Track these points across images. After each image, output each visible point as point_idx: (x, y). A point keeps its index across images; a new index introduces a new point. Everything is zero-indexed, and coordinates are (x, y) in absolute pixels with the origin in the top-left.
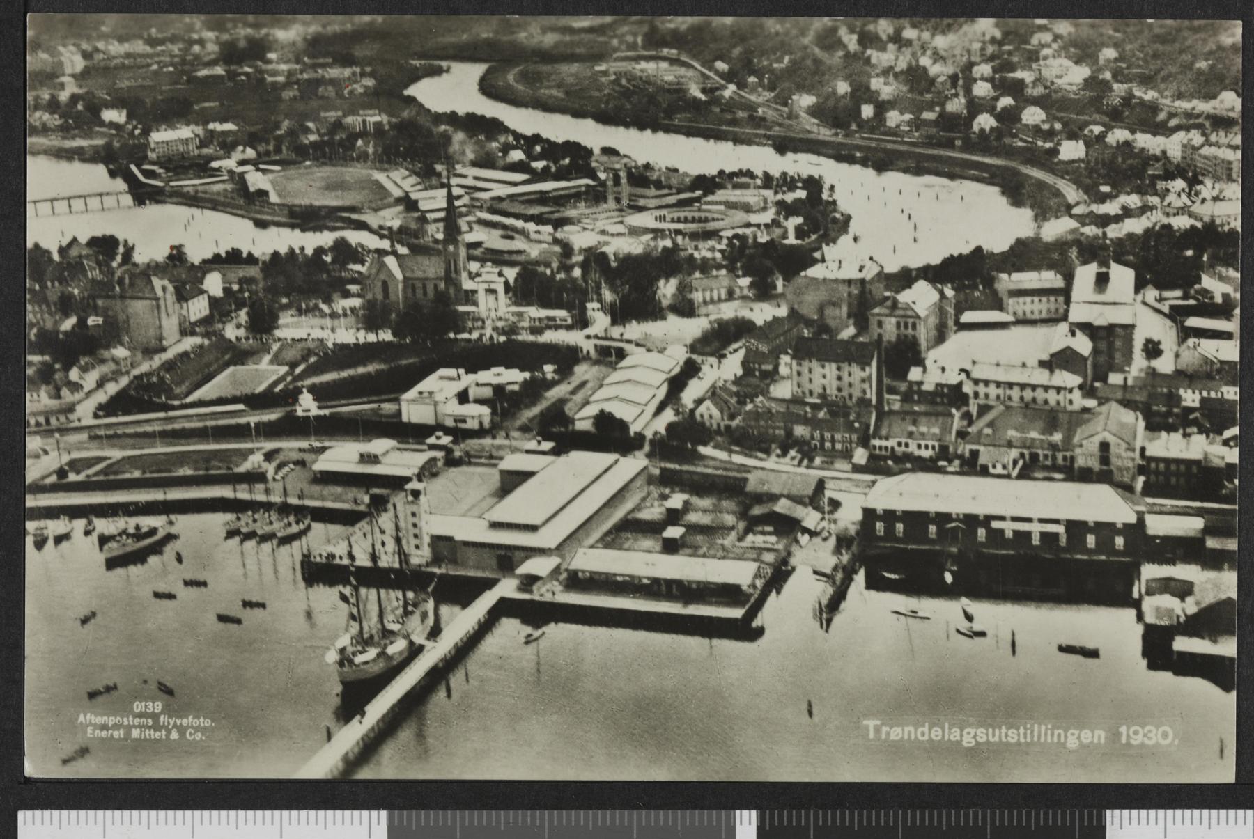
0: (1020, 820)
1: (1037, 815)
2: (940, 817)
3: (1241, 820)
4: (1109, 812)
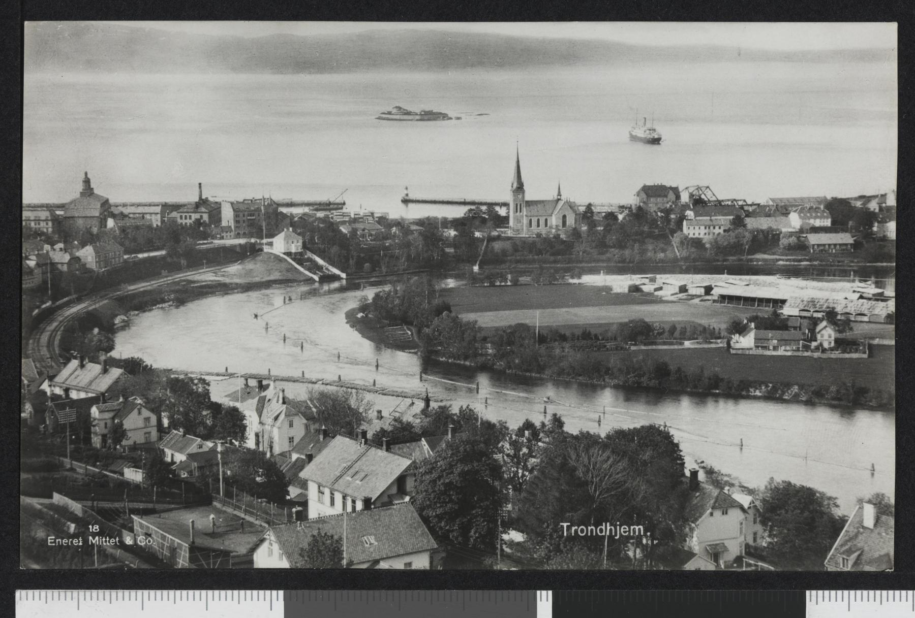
3: (904, 598)
4: (808, 592)
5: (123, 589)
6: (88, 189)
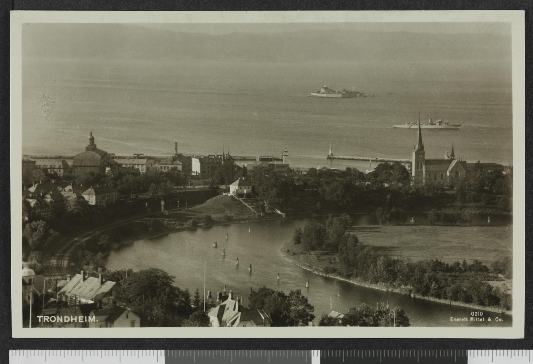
0: (431, 354)
1: (439, 352)
2: (398, 353)
5: (72, 349)
6: (92, 147)
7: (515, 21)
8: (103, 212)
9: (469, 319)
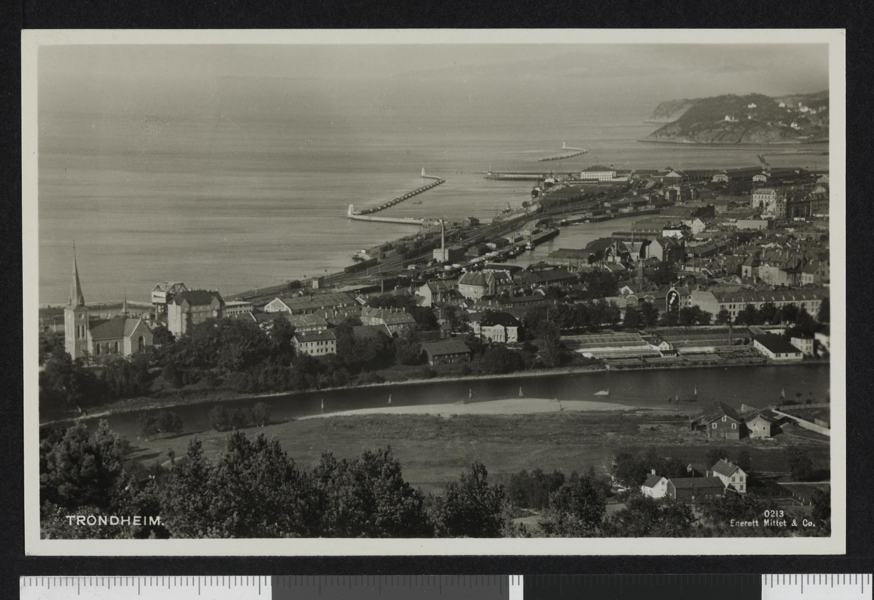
4: (763, 576)
7: (834, 40)
8: (207, 411)
9: (761, 521)
